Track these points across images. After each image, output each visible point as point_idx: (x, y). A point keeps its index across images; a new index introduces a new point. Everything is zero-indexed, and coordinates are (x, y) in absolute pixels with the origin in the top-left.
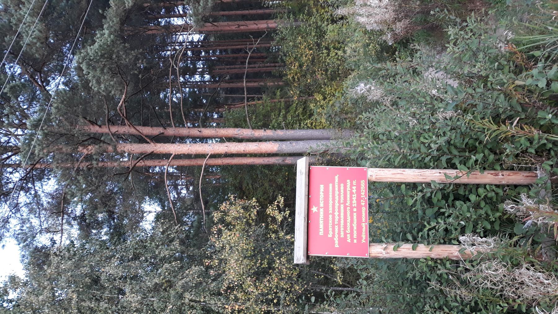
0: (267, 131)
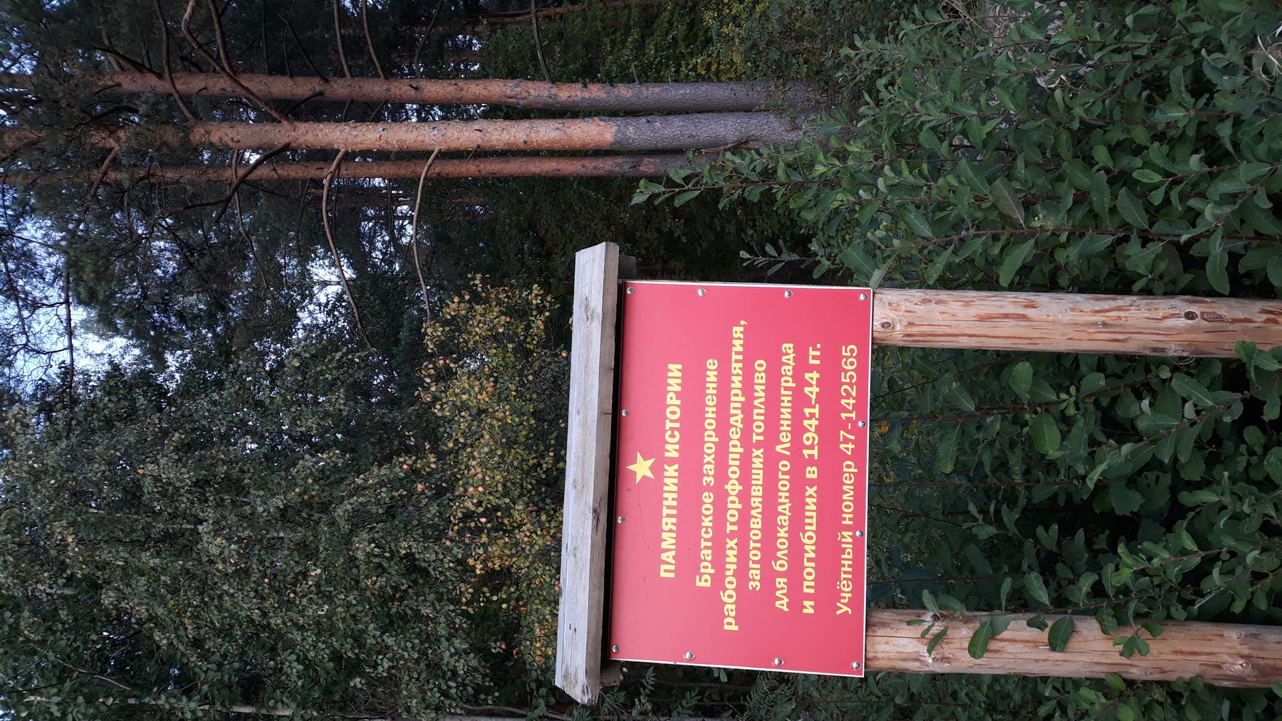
0: (590, 86)
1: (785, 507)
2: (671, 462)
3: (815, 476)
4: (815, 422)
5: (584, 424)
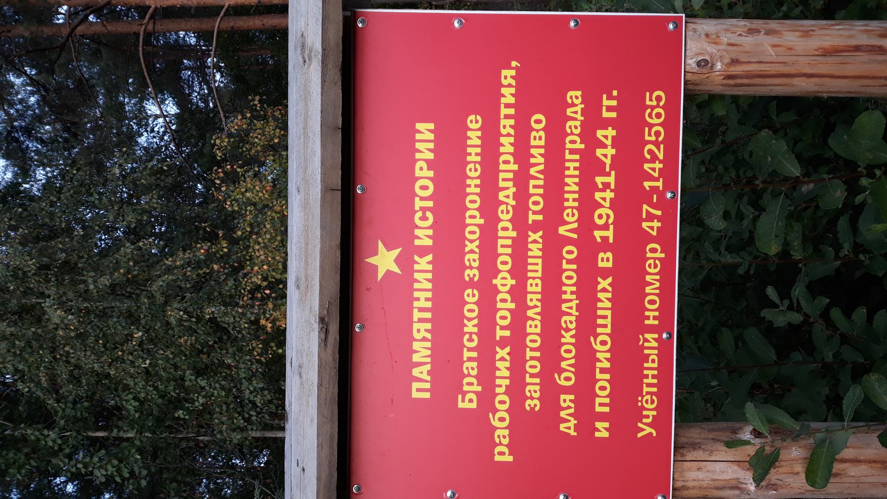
1: (570, 305)
2: (423, 251)
3: (610, 265)
4: (609, 195)
5: (305, 205)
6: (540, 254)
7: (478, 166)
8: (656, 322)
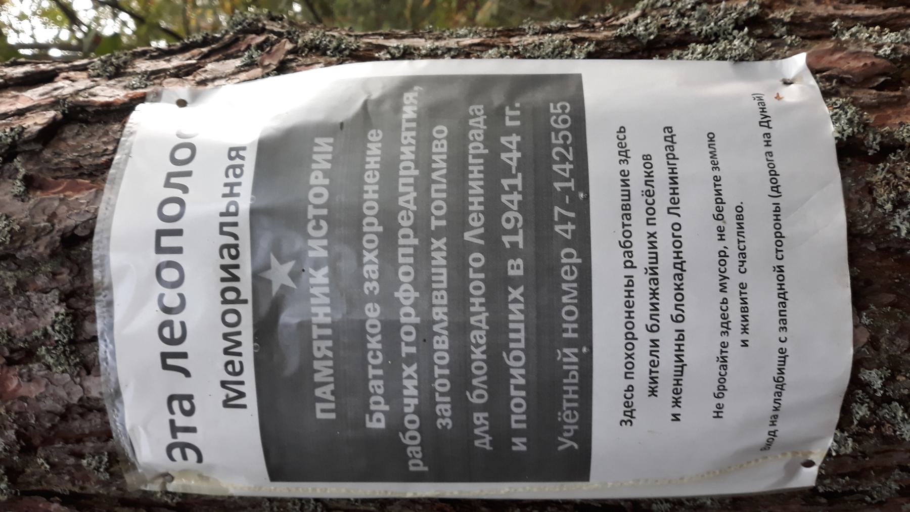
1: (479, 317)
3: (521, 272)
4: (516, 197)
6: (444, 262)
7: (377, 173)
8: (576, 335)
